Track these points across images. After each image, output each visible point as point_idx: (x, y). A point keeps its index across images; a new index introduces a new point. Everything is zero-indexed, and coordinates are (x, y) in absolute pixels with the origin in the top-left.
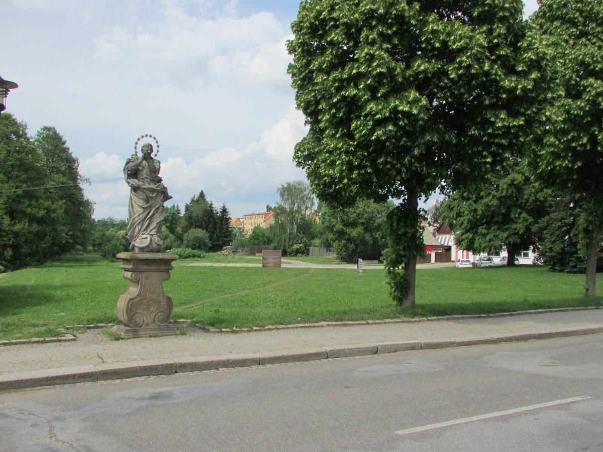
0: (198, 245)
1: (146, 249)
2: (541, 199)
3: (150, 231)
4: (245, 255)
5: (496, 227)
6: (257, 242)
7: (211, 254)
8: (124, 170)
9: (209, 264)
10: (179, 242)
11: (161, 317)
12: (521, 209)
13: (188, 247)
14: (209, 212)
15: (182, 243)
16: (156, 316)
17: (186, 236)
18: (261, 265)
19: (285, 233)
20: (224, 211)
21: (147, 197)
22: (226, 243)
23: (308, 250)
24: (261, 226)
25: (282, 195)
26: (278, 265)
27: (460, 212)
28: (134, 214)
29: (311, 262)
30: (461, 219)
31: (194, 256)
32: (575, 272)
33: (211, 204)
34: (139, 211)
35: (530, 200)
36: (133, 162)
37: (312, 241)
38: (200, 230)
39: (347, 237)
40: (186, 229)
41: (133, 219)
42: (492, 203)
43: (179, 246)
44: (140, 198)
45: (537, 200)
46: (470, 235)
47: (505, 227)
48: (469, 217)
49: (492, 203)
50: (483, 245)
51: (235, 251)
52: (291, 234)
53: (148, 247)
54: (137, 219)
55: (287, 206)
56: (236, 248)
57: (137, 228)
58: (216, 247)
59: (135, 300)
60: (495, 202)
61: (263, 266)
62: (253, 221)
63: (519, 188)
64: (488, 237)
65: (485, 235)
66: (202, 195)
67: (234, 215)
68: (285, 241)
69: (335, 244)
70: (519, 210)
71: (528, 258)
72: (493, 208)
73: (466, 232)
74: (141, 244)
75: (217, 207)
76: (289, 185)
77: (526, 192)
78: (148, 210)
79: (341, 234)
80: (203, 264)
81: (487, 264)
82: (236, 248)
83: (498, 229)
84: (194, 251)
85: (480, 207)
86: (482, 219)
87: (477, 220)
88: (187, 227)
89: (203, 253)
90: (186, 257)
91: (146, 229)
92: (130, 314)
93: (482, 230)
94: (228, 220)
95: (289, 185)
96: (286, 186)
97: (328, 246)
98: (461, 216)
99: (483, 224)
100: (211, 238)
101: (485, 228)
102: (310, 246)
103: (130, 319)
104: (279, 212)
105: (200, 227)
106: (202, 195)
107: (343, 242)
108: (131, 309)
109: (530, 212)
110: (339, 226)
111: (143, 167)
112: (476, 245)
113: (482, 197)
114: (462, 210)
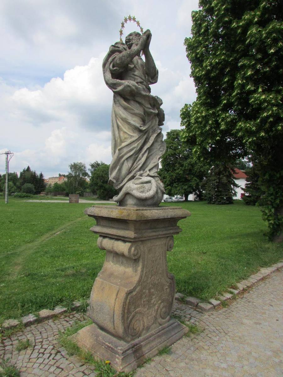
0: (29, 191)
1: (149, 202)
2: (203, 171)
3: (150, 170)
4: (52, 196)
5: (182, 183)
6: (57, 190)
7: (36, 196)
8: (104, 65)
9: (38, 201)
10: (19, 189)
11: (164, 310)
12: (193, 175)
13: (24, 192)
14: (34, 176)
15: (21, 190)
16: (158, 309)
17: (22, 187)
18: (68, 202)
19: (72, 186)
20: (41, 175)
21: (145, 112)
22: (43, 190)
23: (83, 194)
24: (58, 183)
25: (71, 168)
26: (77, 202)
27: (164, 177)
28: (122, 142)
29: (86, 200)
30: (165, 180)
31: (27, 197)
32: (220, 204)
33: (35, 172)
34: (132, 136)
35: (198, 171)
36: (120, 52)
37: (85, 190)
38: (30, 184)
39: (104, 188)
40: (23, 184)
41: (119, 150)
42: (180, 172)
43: (19, 192)
44: (135, 114)
45: (200, 171)
46: (169, 187)
47: (186, 184)
48: (169, 179)
49: (180, 172)
50: (176, 192)
51: (47, 194)
52: (75, 187)
53: (153, 197)
54: (125, 150)
55: (73, 174)
56: (48, 193)
57: (125, 164)
58: (38, 192)
59: (134, 293)
60: (181, 172)
61: (70, 202)
62: (54, 181)
63: (193, 165)
64: (178, 188)
65: (176, 187)
66: (29, 168)
67: (46, 177)
68: (72, 190)
69: (98, 192)
70: (192, 176)
71: (191, 197)
72: (181, 175)
73: (168, 186)
74: (142, 192)
75: (38, 173)
76: (75, 164)
77: (195, 168)
78: (145, 137)
79: (101, 187)
80: (31, 201)
81: (170, 200)
82: (48, 193)
83: (183, 184)
84: (27, 194)
85: (174, 175)
86: (175, 180)
87: (173, 180)
88: (23, 183)
89: (32, 195)
90: (23, 197)
91: (143, 168)
92: (128, 318)
93: (175, 185)
94: (43, 180)
95: (75, 164)
96: (73, 164)
97: (94, 192)
98: (165, 179)
99: (175, 182)
100: (35, 188)
101: (177, 184)
102: (84, 192)
103: (128, 327)
104: (69, 177)
105: (30, 183)
106: (29, 168)
107: (102, 190)
108: (128, 309)
109: (197, 177)
110: (100, 183)
111: (135, 67)
112: (172, 192)
113: (175, 170)
114: (166, 176)
